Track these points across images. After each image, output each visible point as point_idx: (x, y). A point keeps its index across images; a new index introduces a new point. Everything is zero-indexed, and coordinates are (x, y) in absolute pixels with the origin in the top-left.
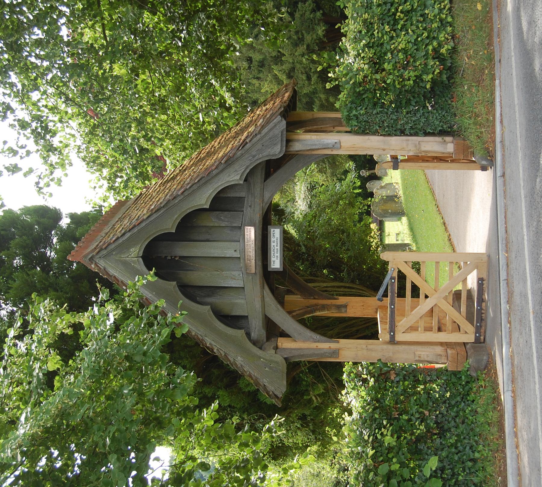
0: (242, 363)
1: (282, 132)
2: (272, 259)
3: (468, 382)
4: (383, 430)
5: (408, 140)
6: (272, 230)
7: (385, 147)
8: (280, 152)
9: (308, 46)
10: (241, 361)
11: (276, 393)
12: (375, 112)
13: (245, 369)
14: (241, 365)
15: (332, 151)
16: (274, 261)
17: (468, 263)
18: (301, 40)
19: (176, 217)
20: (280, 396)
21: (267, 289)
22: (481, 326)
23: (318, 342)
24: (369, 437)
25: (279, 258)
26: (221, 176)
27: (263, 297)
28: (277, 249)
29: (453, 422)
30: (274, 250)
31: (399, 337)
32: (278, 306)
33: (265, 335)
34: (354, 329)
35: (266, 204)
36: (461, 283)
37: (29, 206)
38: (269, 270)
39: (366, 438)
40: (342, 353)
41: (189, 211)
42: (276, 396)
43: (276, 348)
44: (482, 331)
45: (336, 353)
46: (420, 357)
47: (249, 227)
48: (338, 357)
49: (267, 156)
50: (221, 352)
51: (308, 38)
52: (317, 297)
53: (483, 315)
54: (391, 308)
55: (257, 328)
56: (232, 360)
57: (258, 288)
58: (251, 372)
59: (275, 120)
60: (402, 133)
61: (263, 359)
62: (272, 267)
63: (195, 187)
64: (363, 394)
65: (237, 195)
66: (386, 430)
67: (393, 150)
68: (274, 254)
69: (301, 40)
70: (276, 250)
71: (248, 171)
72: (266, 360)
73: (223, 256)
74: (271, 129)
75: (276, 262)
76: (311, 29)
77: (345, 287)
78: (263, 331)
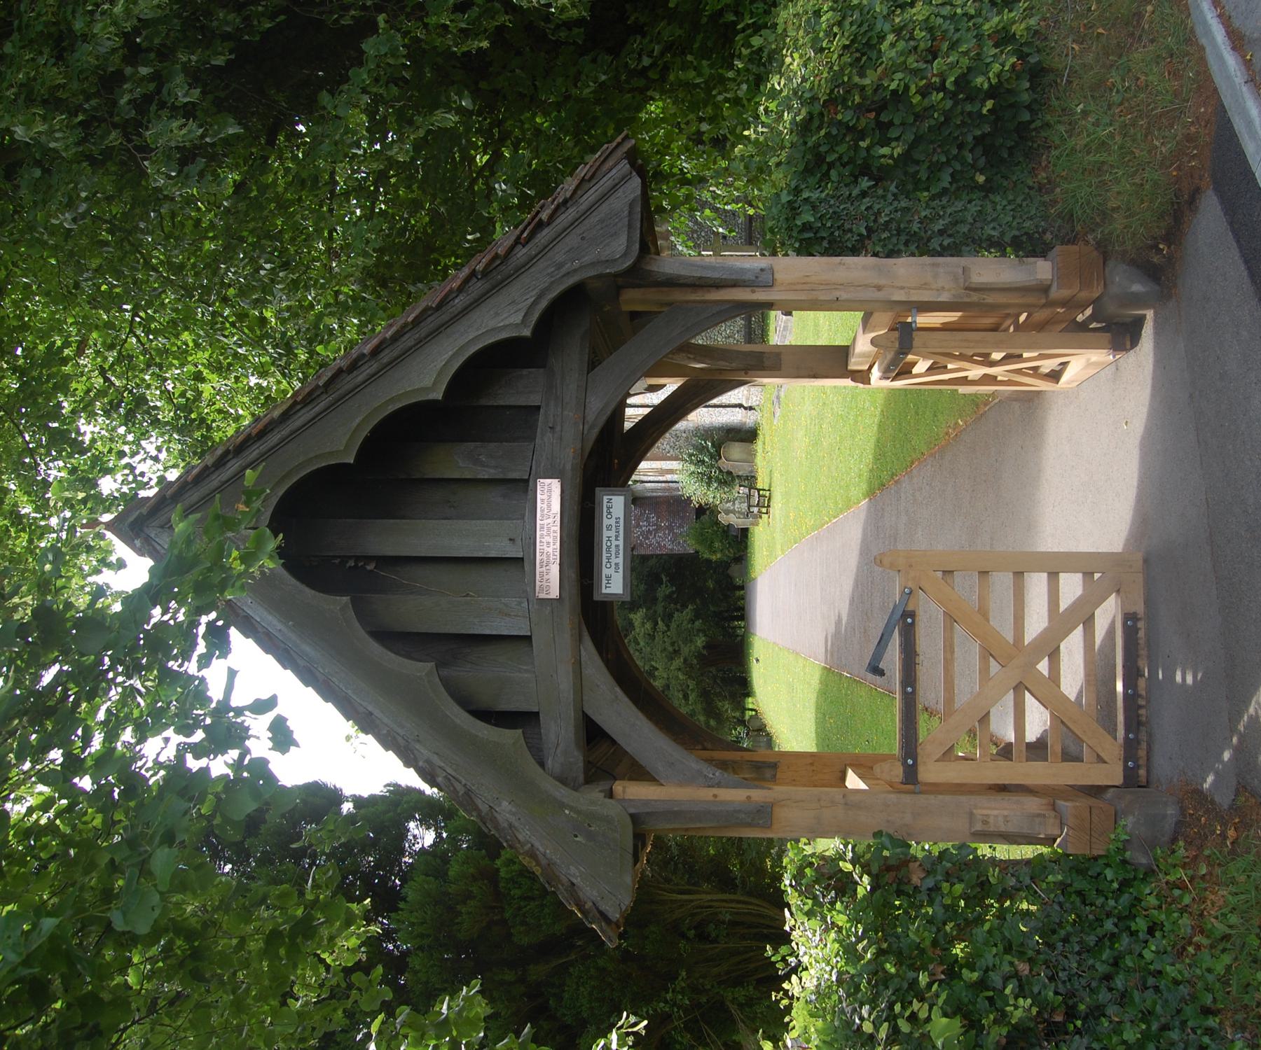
0: (513, 819)
1: (631, 205)
2: (605, 571)
3: (1125, 884)
4: (916, 1005)
5: (937, 265)
6: (605, 498)
7: (882, 282)
8: (625, 255)
9: (685, 660)
10: (510, 812)
11: (603, 907)
12: (855, 192)
13: (520, 837)
14: (511, 825)
15: (753, 292)
16: (609, 578)
17: (1097, 576)
18: (677, 652)
19: (357, 421)
20: (615, 915)
21: (589, 648)
22: (1137, 741)
23: (719, 785)
24: (877, 1027)
25: (621, 570)
26: (475, 315)
27: (578, 665)
28: (617, 546)
29: (1104, 990)
30: (609, 547)
31: (930, 772)
32: (618, 689)
33: (581, 764)
34: (752, 966)
35: (591, 427)
36: (1081, 627)
37: (139, 586)
38: (596, 598)
39: (868, 1027)
40: (782, 814)
41: (391, 409)
42: (604, 916)
43: (610, 794)
44: (1142, 753)
45: (763, 814)
46: (985, 822)
47: (548, 481)
48: (769, 827)
49: (593, 264)
50: (457, 785)
51: (685, 650)
52: (709, 746)
53: (1142, 712)
54: (904, 692)
55: (560, 734)
56: (484, 808)
57: (566, 639)
58: (537, 844)
59: (614, 171)
60: (924, 249)
61: (571, 809)
62: (604, 591)
63: (408, 340)
64: (841, 920)
65: (522, 401)
66: (926, 1006)
67: (902, 288)
68: (608, 558)
69: (677, 652)
70: (613, 549)
71: (544, 304)
72: (579, 812)
73: (481, 555)
74: (604, 198)
75: (613, 580)
76: (689, 640)
77: (739, 902)
78: (576, 753)
